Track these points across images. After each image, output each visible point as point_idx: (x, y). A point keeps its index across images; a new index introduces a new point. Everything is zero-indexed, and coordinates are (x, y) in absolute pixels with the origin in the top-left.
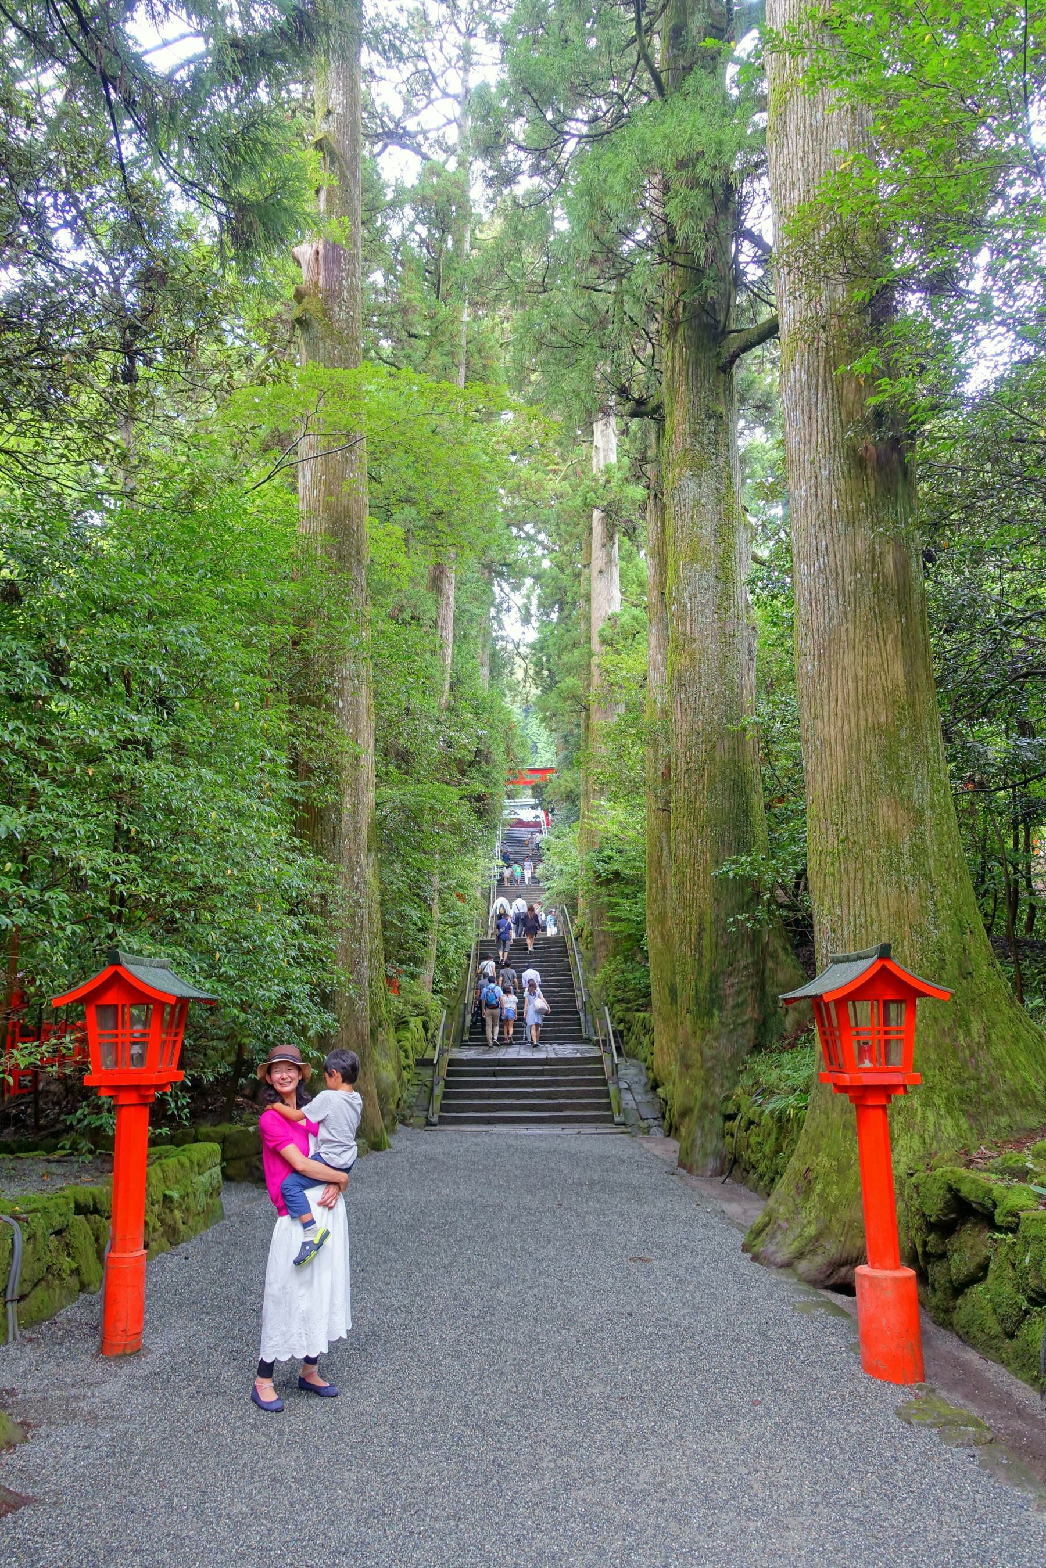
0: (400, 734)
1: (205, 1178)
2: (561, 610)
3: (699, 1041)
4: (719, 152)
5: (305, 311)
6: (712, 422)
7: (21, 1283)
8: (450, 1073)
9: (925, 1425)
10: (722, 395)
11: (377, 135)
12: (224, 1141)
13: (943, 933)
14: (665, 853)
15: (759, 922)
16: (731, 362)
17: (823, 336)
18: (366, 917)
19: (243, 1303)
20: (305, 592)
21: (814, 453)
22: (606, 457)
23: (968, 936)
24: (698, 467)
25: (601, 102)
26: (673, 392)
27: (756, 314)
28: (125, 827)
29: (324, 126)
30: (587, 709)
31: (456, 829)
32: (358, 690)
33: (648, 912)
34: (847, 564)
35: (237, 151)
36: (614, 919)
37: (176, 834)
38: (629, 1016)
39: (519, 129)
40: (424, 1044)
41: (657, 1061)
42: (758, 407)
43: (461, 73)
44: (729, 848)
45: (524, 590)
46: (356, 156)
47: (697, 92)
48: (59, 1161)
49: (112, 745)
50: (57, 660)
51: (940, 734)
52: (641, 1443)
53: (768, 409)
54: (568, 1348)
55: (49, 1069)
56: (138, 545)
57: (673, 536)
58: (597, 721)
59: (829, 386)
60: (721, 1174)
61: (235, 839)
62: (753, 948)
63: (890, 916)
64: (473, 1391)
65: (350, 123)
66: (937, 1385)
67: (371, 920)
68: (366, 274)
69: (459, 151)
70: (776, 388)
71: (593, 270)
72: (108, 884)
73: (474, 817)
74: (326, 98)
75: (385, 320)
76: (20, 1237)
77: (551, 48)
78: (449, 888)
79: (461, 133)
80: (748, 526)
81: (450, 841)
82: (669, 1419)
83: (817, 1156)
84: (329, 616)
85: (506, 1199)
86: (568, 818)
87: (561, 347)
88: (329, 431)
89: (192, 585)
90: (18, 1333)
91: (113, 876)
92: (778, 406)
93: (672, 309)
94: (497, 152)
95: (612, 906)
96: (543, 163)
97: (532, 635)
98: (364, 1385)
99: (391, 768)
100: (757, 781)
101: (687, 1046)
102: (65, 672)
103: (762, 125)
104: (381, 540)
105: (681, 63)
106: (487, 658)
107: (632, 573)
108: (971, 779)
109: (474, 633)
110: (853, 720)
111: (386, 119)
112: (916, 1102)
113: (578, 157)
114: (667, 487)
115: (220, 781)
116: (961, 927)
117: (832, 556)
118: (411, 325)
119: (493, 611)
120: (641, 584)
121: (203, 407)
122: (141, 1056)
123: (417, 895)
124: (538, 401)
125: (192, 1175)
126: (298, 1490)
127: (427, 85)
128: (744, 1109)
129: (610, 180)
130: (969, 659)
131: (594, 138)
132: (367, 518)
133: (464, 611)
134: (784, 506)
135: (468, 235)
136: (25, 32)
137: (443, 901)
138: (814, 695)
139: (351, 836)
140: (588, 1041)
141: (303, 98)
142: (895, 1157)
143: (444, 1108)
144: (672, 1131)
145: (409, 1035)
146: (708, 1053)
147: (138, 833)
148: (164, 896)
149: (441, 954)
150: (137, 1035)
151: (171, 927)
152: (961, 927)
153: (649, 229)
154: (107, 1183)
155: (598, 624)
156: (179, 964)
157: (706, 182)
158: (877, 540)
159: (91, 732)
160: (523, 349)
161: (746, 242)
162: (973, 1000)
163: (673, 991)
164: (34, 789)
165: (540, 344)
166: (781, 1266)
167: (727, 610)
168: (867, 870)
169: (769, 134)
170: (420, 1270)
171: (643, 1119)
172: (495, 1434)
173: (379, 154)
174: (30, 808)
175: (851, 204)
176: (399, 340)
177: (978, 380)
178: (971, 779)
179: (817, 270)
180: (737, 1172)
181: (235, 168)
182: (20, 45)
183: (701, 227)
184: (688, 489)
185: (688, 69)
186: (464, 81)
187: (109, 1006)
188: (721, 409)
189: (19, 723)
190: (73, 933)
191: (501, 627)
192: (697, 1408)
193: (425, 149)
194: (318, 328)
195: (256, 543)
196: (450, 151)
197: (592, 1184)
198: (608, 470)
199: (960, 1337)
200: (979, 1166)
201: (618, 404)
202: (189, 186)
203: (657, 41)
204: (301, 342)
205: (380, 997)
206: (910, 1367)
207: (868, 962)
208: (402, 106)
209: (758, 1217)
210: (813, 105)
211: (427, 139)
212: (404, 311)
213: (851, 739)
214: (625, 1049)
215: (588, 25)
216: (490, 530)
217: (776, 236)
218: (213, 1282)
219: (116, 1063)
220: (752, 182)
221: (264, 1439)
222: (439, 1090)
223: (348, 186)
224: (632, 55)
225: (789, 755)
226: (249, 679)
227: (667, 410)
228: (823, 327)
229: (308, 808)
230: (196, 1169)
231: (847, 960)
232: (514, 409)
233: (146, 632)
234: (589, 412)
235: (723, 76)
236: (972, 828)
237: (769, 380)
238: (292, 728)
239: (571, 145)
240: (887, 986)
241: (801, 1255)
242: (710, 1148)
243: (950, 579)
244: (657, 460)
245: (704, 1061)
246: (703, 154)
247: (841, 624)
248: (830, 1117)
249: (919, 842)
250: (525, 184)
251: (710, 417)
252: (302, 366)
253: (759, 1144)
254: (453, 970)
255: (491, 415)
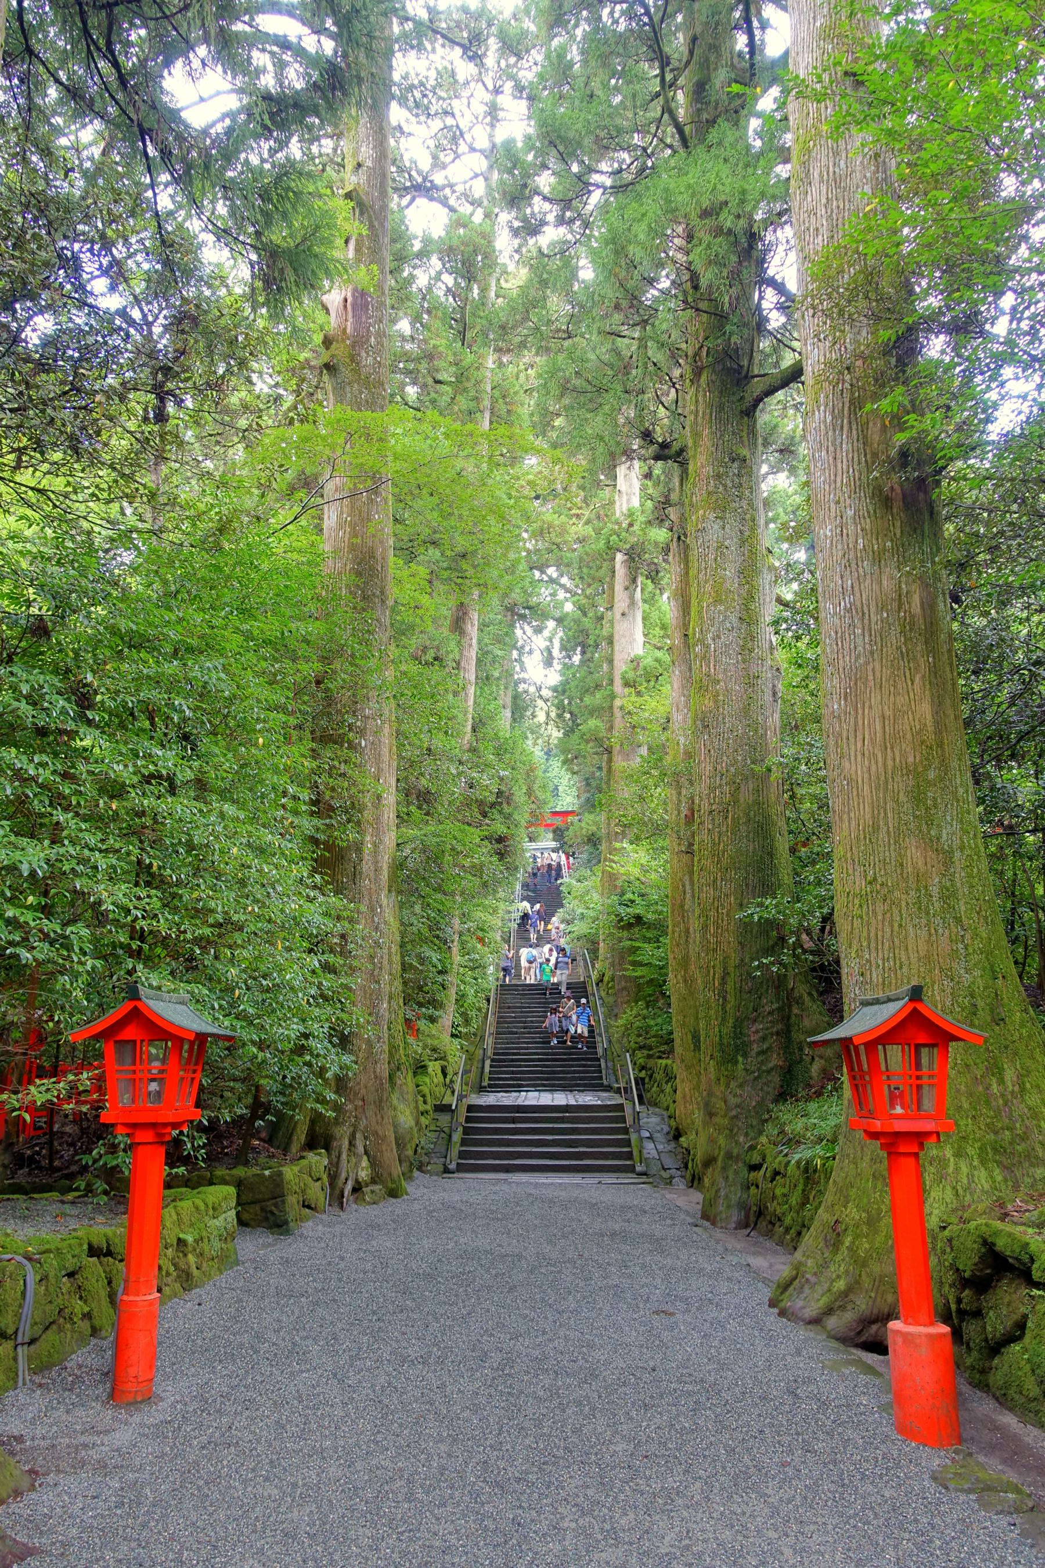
0: (422, 774)
1: (220, 1222)
2: (583, 653)
3: (722, 1088)
4: (742, 201)
5: (333, 356)
6: (736, 465)
7: (32, 1326)
8: (468, 1119)
9: (962, 1491)
10: (745, 439)
11: (406, 189)
12: (239, 1184)
13: (974, 978)
14: (688, 896)
15: (785, 966)
16: (755, 406)
17: (847, 377)
18: (386, 957)
19: (256, 1352)
20: (331, 631)
21: (839, 493)
22: (628, 501)
23: (1000, 981)
24: (721, 509)
25: (625, 155)
26: (696, 435)
27: (779, 359)
28: (147, 861)
29: (353, 178)
30: (609, 751)
31: (477, 870)
32: (380, 729)
33: (671, 956)
34: (873, 604)
35: (270, 200)
36: (635, 964)
37: (197, 872)
38: (651, 1063)
39: (545, 181)
40: (443, 1090)
41: (680, 1110)
42: (781, 451)
43: (488, 128)
44: (753, 891)
45: (546, 633)
46: (384, 207)
47: (720, 143)
48: (73, 1203)
49: (136, 779)
50: (83, 695)
51: (969, 774)
52: (666, 1504)
53: (791, 452)
54: (589, 1403)
55: (66, 1106)
56: (165, 583)
57: (697, 577)
58: (619, 763)
59: (854, 427)
60: (747, 1226)
61: (256, 875)
62: (777, 994)
63: (919, 960)
64: (491, 1446)
65: (379, 176)
66: (974, 1449)
67: (390, 962)
68: (394, 321)
69: (486, 203)
70: (799, 432)
71: (617, 317)
72: (129, 918)
73: (495, 858)
74: (356, 152)
75: (411, 366)
76: (32, 1278)
77: (577, 103)
78: (469, 931)
79: (488, 187)
80: (771, 568)
81: (470, 883)
82: (695, 1479)
83: (845, 1207)
84: (353, 656)
85: (526, 1248)
86: (589, 861)
87: (583, 392)
88: (356, 472)
89: (217, 622)
90: (28, 1378)
91: (134, 912)
92: (803, 450)
93: (696, 355)
94: (522, 204)
95: (634, 950)
96: (568, 214)
97: (553, 677)
98: (379, 1437)
99: (413, 808)
100: (781, 823)
101: (710, 1094)
102: (91, 706)
103: (785, 175)
104: (404, 582)
105: (705, 116)
106: (509, 701)
107: (655, 616)
108: (1000, 823)
109: (496, 674)
110: (880, 759)
111: (414, 173)
112: (948, 1153)
113: (604, 208)
114: (690, 528)
115: (242, 817)
116: (993, 972)
117: (858, 595)
118: (437, 371)
119: (515, 654)
120: (664, 627)
121: (231, 452)
122: (158, 1093)
123: (438, 937)
124: (562, 445)
125: (207, 1219)
126: (311, 1546)
127: (454, 140)
128: (769, 1159)
129: (634, 228)
130: (998, 700)
131: (619, 189)
132: (392, 559)
133: (487, 653)
134: (807, 551)
135: (493, 284)
136: (67, 88)
137: (463, 944)
138: (840, 734)
139: (372, 874)
140: (608, 1088)
141: (333, 152)
142: (927, 1209)
143: (462, 1155)
144: (695, 1181)
145: (427, 1080)
146: (733, 1101)
147: (159, 868)
148: (185, 932)
149: (461, 997)
150: (154, 1071)
151: (191, 964)
152: (993, 972)
153: (673, 277)
154: (121, 1225)
155: (621, 667)
156: (198, 1001)
157: (730, 231)
158: (903, 579)
159: (115, 766)
160: (548, 393)
161: (770, 289)
162: (1006, 1047)
163: (696, 1038)
164: (58, 823)
165: (565, 389)
166: (810, 1323)
167: (751, 651)
168: (895, 911)
169: (792, 182)
170: (437, 1320)
171: (665, 1169)
172: (515, 1492)
173: (407, 207)
174: (53, 842)
175: (877, 245)
176: (424, 386)
177: (1006, 420)
178: (1000, 823)
179: (841, 313)
180: (763, 1224)
181: (267, 215)
182: (60, 102)
183: (725, 274)
184: (712, 531)
185: (712, 122)
186: (491, 136)
187: (127, 1042)
188: (745, 452)
189: (45, 758)
190: (93, 968)
191: (523, 669)
192: (724, 1468)
193: (452, 202)
194: (345, 372)
195: (283, 582)
196: (475, 203)
197: (613, 1235)
198: (631, 514)
199: (997, 1399)
200: (1015, 1219)
201: (641, 447)
202: (222, 234)
203: (680, 96)
204: (329, 387)
205: (399, 1041)
206: (949, 1430)
207: (900, 1004)
208: (430, 160)
209: (785, 1271)
210: (836, 153)
211: (454, 192)
212: (430, 356)
213: (878, 778)
214: (647, 1096)
215: (613, 82)
216: (513, 573)
217: (801, 281)
218: (227, 1329)
219: (134, 1101)
220: (775, 231)
221: (276, 1491)
222: (457, 1137)
223: (377, 236)
224: (655, 110)
225: (814, 797)
226: (273, 715)
227: (691, 453)
228: (848, 368)
229: (329, 847)
230: (211, 1212)
231: (877, 1002)
232: (538, 452)
233: (172, 668)
234: (612, 455)
235: (746, 128)
236: (1001, 874)
237: (791, 424)
238: (315, 764)
239: (596, 197)
240: (919, 1029)
241: (829, 1311)
242: (734, 1199)
243: (978, 621)
244: (681, 504)
245: (729, 1109)
246: (726, 203)
247: (867, 663)
248: (860, 1163)
249: (948, 884)
250: (551, 235)
251: (733, 460)
252: (329, 409)
253: (785, 1195)
254: (473, 1013)
255: (514, 460)
